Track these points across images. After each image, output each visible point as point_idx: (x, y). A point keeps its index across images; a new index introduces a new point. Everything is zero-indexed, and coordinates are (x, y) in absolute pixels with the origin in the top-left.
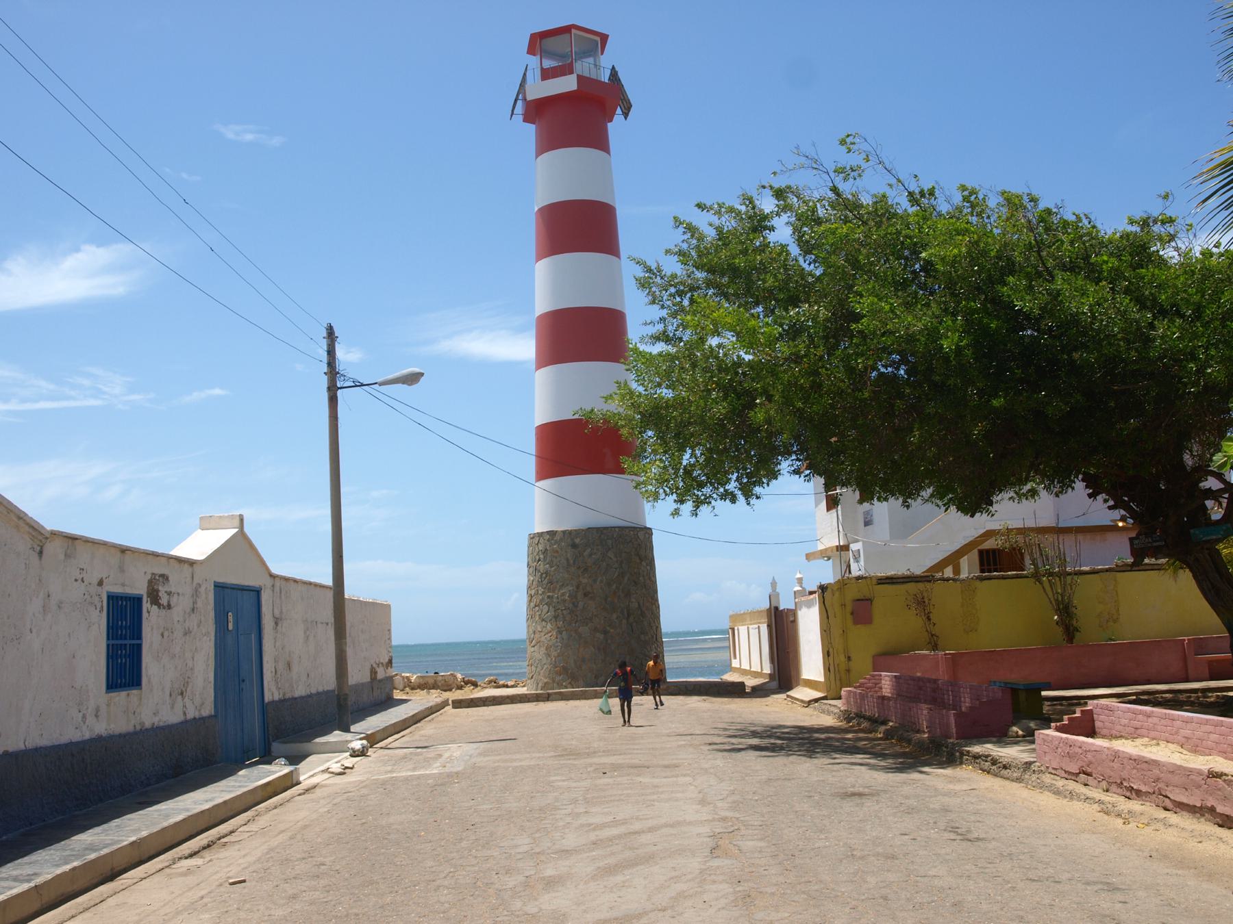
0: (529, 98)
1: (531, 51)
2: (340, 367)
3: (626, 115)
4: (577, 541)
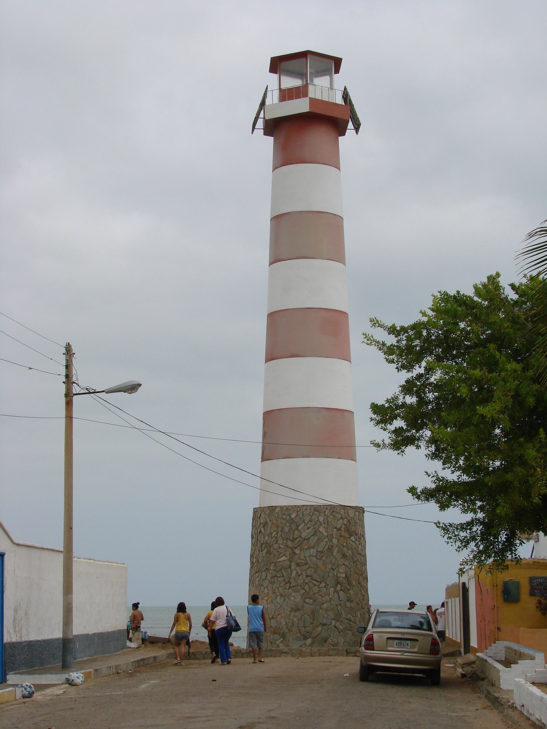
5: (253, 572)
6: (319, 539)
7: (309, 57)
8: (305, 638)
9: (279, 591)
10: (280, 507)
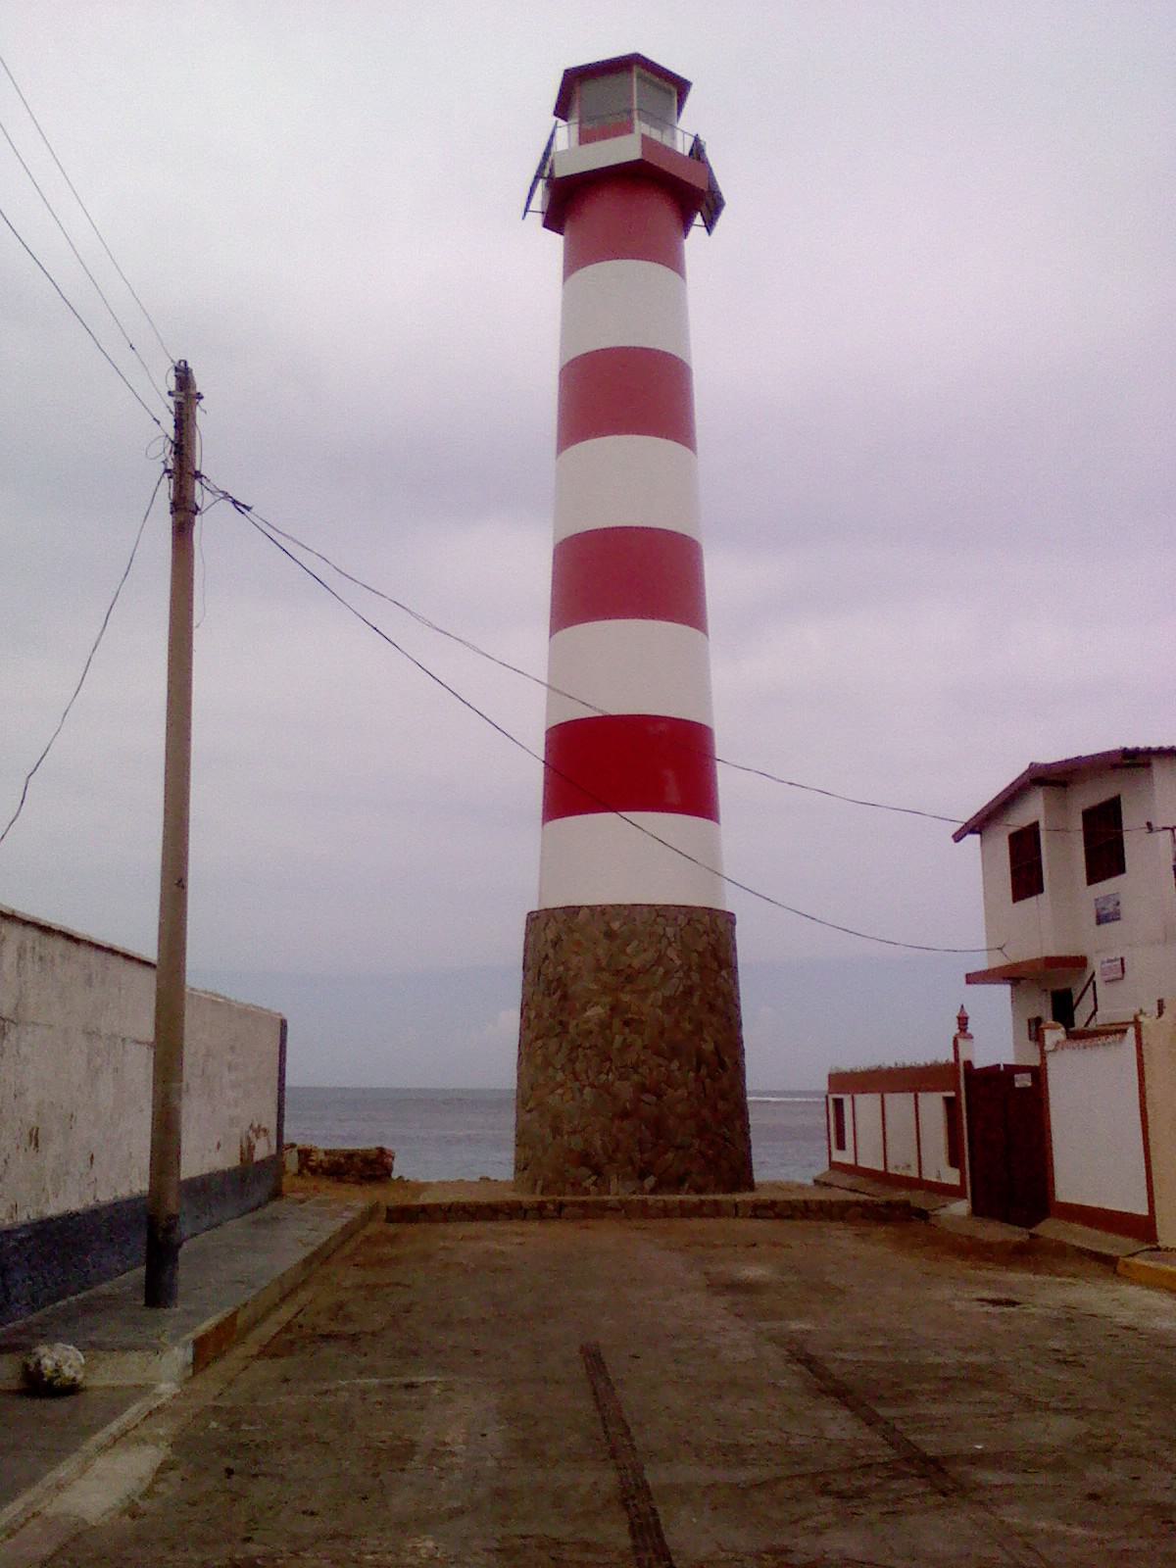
0: (558, 174)
1: (562, 110)
2: (205, 458)
3: (709, 225)
4: (616, 925)
5: (530, 1035)
6: (666, 973)
7: (636, 70)
8: (642, 1176)
9: (588, 1078)
10: (588, 907)
